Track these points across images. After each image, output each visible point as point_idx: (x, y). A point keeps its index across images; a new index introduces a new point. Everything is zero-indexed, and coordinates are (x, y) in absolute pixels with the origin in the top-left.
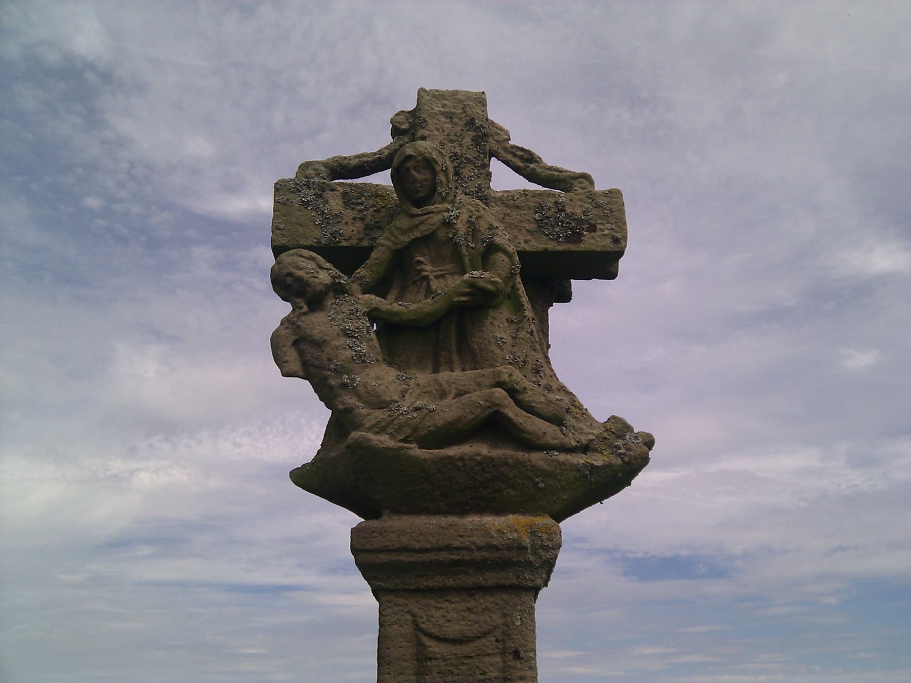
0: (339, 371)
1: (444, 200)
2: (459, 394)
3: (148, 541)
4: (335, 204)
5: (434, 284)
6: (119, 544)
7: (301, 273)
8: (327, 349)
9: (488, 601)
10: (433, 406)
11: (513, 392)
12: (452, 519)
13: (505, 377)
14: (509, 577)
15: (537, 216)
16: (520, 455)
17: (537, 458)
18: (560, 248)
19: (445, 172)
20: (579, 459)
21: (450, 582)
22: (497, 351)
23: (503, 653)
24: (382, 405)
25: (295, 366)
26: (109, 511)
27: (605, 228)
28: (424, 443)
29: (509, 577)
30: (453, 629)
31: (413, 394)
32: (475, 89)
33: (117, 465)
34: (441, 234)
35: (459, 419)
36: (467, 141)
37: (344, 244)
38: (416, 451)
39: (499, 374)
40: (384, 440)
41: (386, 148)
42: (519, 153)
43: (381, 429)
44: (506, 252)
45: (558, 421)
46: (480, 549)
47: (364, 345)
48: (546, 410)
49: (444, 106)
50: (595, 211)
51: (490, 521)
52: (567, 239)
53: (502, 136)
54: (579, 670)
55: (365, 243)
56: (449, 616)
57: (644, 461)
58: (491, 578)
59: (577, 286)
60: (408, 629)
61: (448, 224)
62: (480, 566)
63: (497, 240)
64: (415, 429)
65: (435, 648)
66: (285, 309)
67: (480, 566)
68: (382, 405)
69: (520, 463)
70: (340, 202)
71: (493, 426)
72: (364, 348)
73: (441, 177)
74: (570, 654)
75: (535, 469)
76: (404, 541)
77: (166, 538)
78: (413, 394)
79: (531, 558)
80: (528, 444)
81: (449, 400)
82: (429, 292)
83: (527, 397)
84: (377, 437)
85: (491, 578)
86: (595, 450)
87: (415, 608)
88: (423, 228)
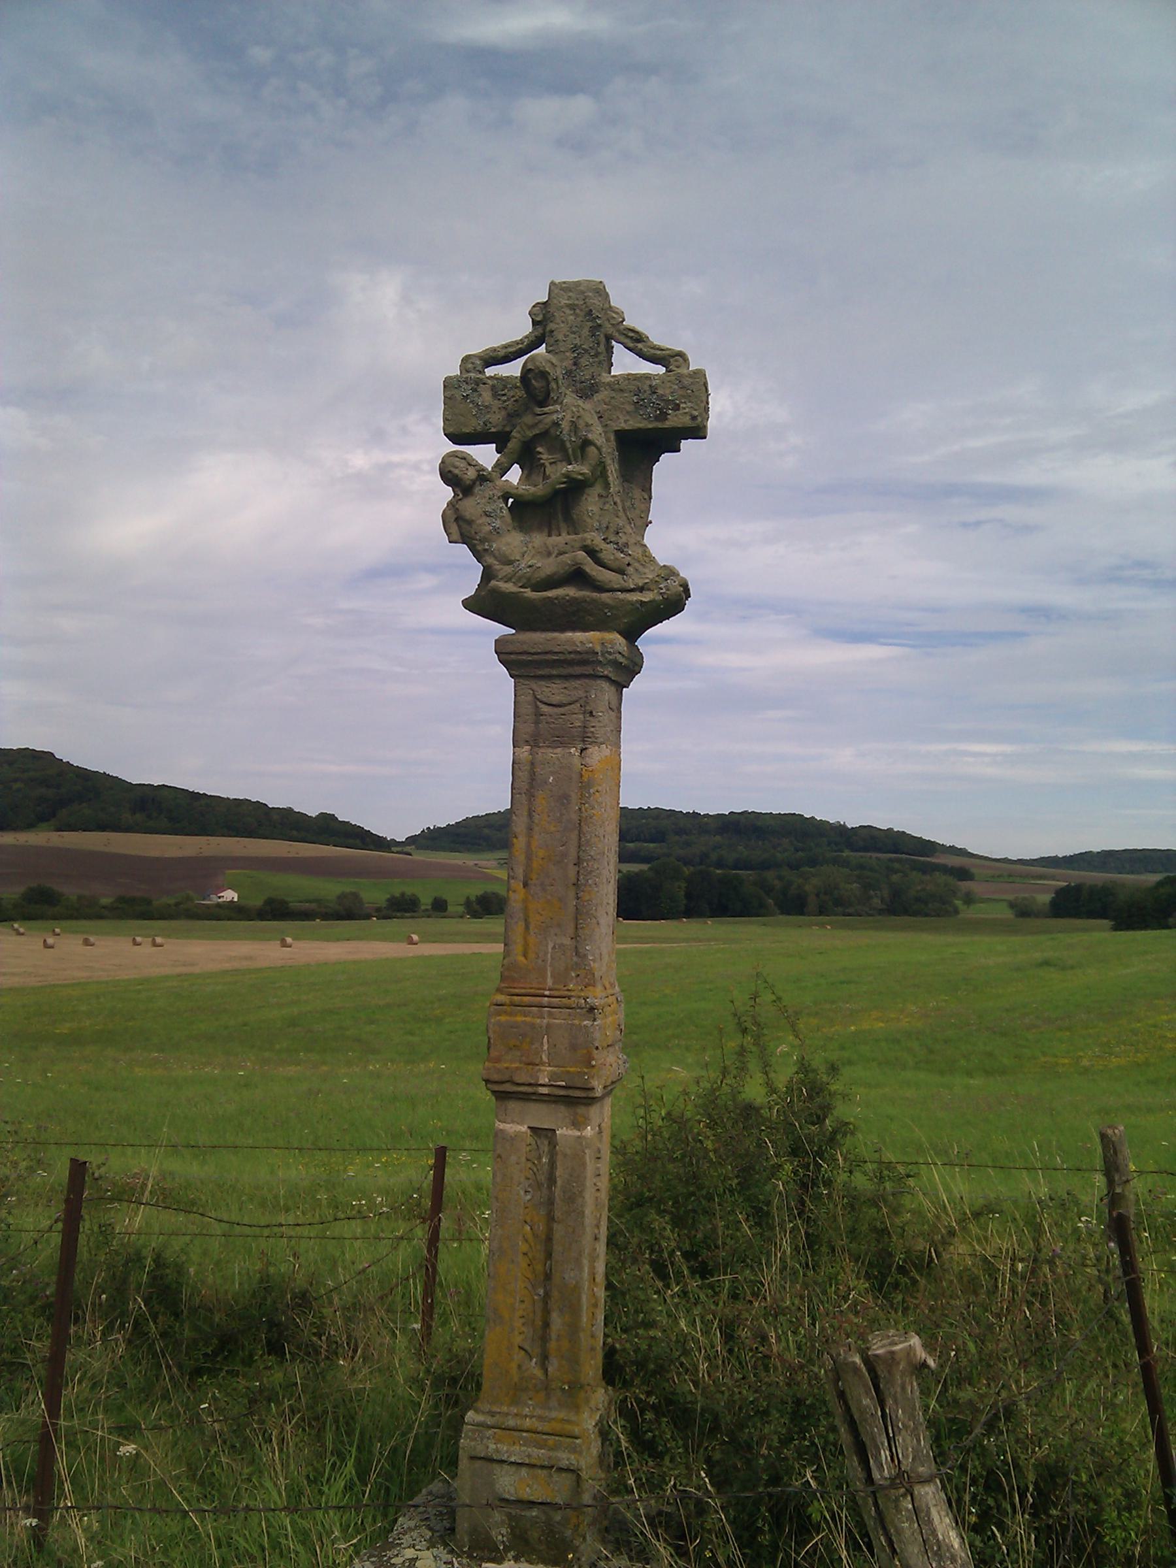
0: (482, 541)
1: (556, 402)
2: (561, 553)
4: (486, 396)
5: (549, 470)
7: (456, 471)
8: (474, 526)
9: (576, 683)
10: (539, 565)
11: (592, 552)
12: (556, 635)
13: (589, 542)
14: (588, 670)
15: (635, 399)
16: (595, 595)
17: (605, 597)
18: (650, 426)
19: (556, 380)
20: (635, 597)
21: (554, 672)
22: (589, 520)
23: (584, 713)
24: (510, 562)
25: (456, 536)
27: (686, 407)
29: (588, 670)
30: (556, 699)
31: (532, 552)
32: (68, 1165)
34: (552, 431)
35: (555, 574)
36: (585, 332)
37: (493, 430)
38: (529, 593)
39: (585, 540)
40: (509, 587)
41: (526, 337)
42: (631, 334)
43: (508, 579)
44: (595, 445)
45: (622, 572)
46: (570, 653)
47: (498, 522)
48: (614, 565)
49: (569, 298)
50: (681, 392)
51: (579, 636)
52: (657, 418)
55: (508, 429)
56: (554, 691)
58: (578, 670)
59: (684, 444)
60: (530, 698)
61: (556, 424)
62: (571, 663)
63: (590, 436)
64: (529, 579)
65: (545, 709)
66: (448, 493)
67: (571, 663)
68: (510, 562)
69: (594, 601)
70: (489, 393)
71: (577, 577)
72: (498, 523)
73: (553, 385)
75: (606, 605)
76: (525, 648)
78: (532, 552)
79: (601, 659)
80: (600, 588)
81: (552, 559)
82: (545, 477)
83: (602, 556)
84: (506, 585)
85: (578, 670)
86: (649, 590)
87: (534, 686)
88: (541, 426)
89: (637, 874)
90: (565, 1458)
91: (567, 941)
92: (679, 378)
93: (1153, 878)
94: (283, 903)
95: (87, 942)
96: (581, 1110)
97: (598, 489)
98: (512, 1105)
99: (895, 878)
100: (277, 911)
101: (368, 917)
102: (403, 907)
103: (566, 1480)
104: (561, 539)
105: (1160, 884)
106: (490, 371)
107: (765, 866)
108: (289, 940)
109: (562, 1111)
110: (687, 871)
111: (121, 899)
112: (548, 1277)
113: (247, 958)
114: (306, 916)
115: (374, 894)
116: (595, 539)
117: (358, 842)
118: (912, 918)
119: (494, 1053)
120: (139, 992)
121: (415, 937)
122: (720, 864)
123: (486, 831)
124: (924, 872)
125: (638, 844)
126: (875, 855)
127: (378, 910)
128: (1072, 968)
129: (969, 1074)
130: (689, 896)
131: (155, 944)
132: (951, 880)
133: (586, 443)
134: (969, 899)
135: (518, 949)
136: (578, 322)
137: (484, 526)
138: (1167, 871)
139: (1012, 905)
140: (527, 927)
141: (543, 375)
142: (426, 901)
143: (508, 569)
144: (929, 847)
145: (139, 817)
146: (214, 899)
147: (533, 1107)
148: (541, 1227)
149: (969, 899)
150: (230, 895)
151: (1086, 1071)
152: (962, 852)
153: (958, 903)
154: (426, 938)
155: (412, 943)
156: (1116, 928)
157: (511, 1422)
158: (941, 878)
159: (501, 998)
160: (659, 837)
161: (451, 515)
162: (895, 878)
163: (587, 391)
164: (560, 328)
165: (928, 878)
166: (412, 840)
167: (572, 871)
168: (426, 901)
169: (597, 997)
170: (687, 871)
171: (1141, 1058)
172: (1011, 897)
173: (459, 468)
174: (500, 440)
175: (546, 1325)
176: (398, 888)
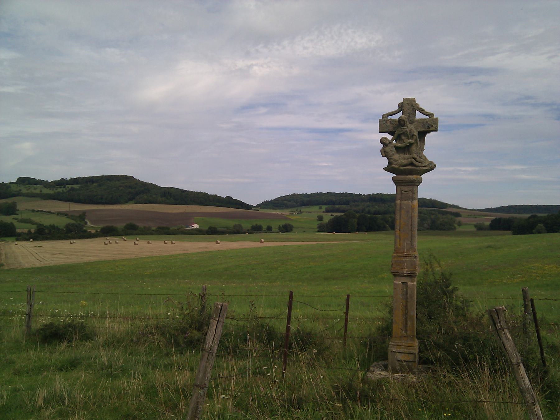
3: (265, 105)
4: (389, 124)
6: (249, 107)
11: (415, 159)
14: (413, 184)
17: (418, 168)
26: (241, 90)
27: (434, 126)
28: (402, 167)
29: (413, 184)
30: (406, 190)
31: (401, 159)
33: (241, 63)
43: (396, 165)
45: (421, 163)
53: (417, 105)
54: (524, 176)
56: (405, 188)
57: (432, 169)
58: (410, 184)
66: (382, 146)
74: (518, 167)
77: (274, 103)
78: (401, 159)
85: (410, 184)
89: (340, 217)
90: (412, 351)
91: (409, 242)
92: (433, 119)
93: (527, 216)
94: (215, 228)
95: (149, 243)
96: (413, 278)
97: (415, 145)
98: (398, 278)
99: (433, 217)
100: (213, 231)
101: (245, 233)
102: (257, 229)
103: (412, 356)
104: (407, 156)
105: (530, 218)
106: (389, 118)
107: (385, 213)
108: (219, 241)
109: (409, 279)
110: (357, 215)
111: (159, 228)
112: (406, 314)
113: (205, 248)
114: (223, 233)
115: (246, 225)
116: (415, 156)
117: (240, 207)
118: (439, 231)
119: (393, 266)
120: (171, 260)
121: (263, 240)
122: (369, 212)
123: (285, 202)
124: (443, 215)
125: (340, 206)
126: (425, 208)
127: (248, 230)
128: (499, 248)
129: (465, 285)
130: (358, 224)
131: (172, 243)
132: (453, 217)
133: (413, 135)
134: (460, 224)
135: (398, 244)
136: (409, 106)
137: (391, 153)
138: (532, 213)
139: (476, 226)
140: (400, 239)
141: (404, 121)
142: (265, 227)
143: (396, 163)
144: (445, 205)
145: (163, 198)
146: (190, 228)
147: (402, 278)
148: (404, 304)
149: (460, 224)
150: (196, 226)
151: (505, 284)
152: (457, 207)
153: (456, 225)
154: (267, 240)
155: (262, 242)
156: (514, 234)
157: (400, 344)
158: (450, 216)
159: (395, 255)
160: (347, 203)
161: (383, 151)
162: (433, 217)
163: (412, 123)
164: (405, 108)
165: (444, 216)
166: (259, 205)
167: (410, 227)
168: (265, 227)
169: (416, 254)
170: (357, 215)
171: (524, 279)
172: (475, 223)
173: (385, 141)
174: (391, 133)
175: (406, 324)
176: (255, 223)
